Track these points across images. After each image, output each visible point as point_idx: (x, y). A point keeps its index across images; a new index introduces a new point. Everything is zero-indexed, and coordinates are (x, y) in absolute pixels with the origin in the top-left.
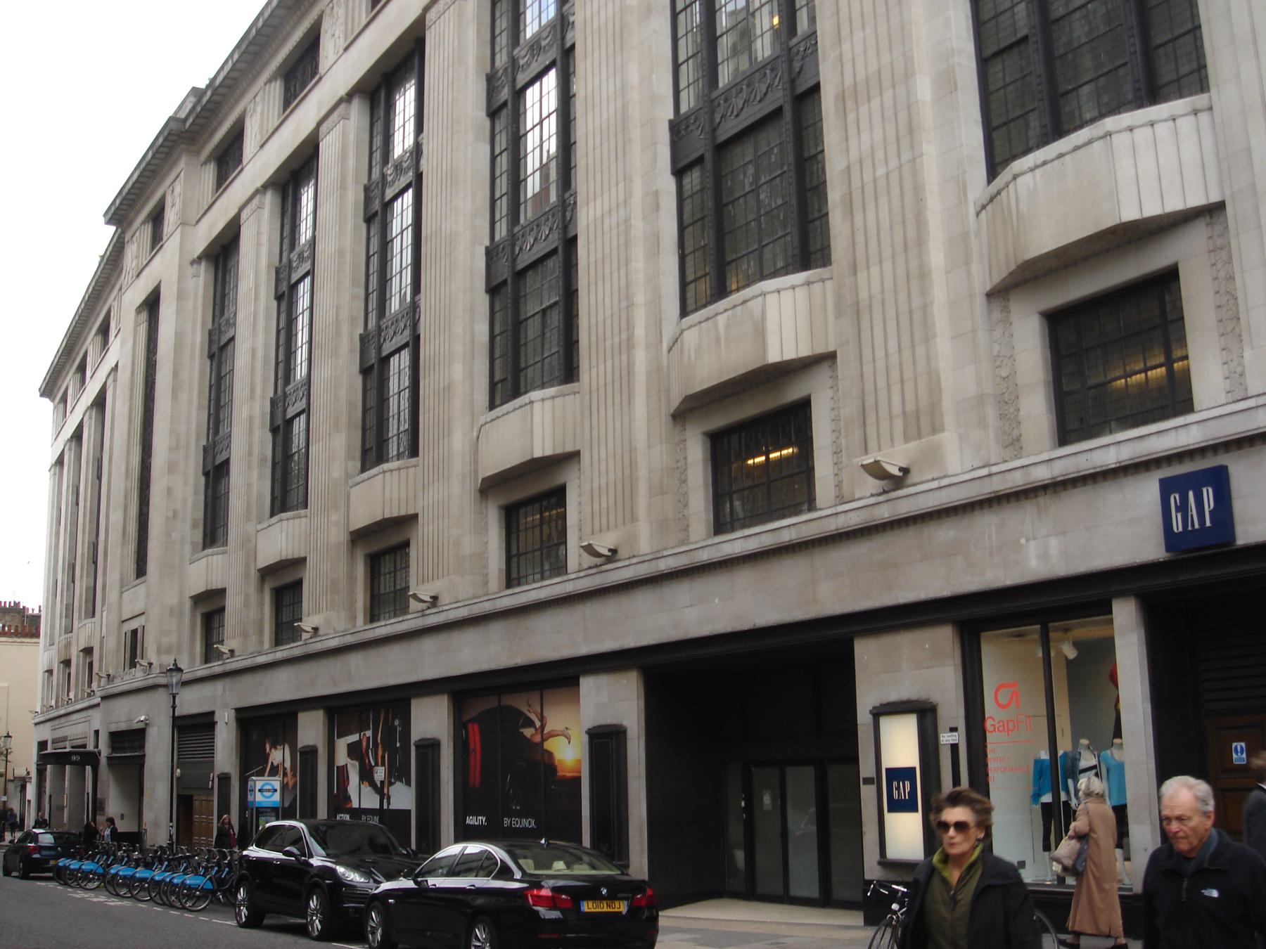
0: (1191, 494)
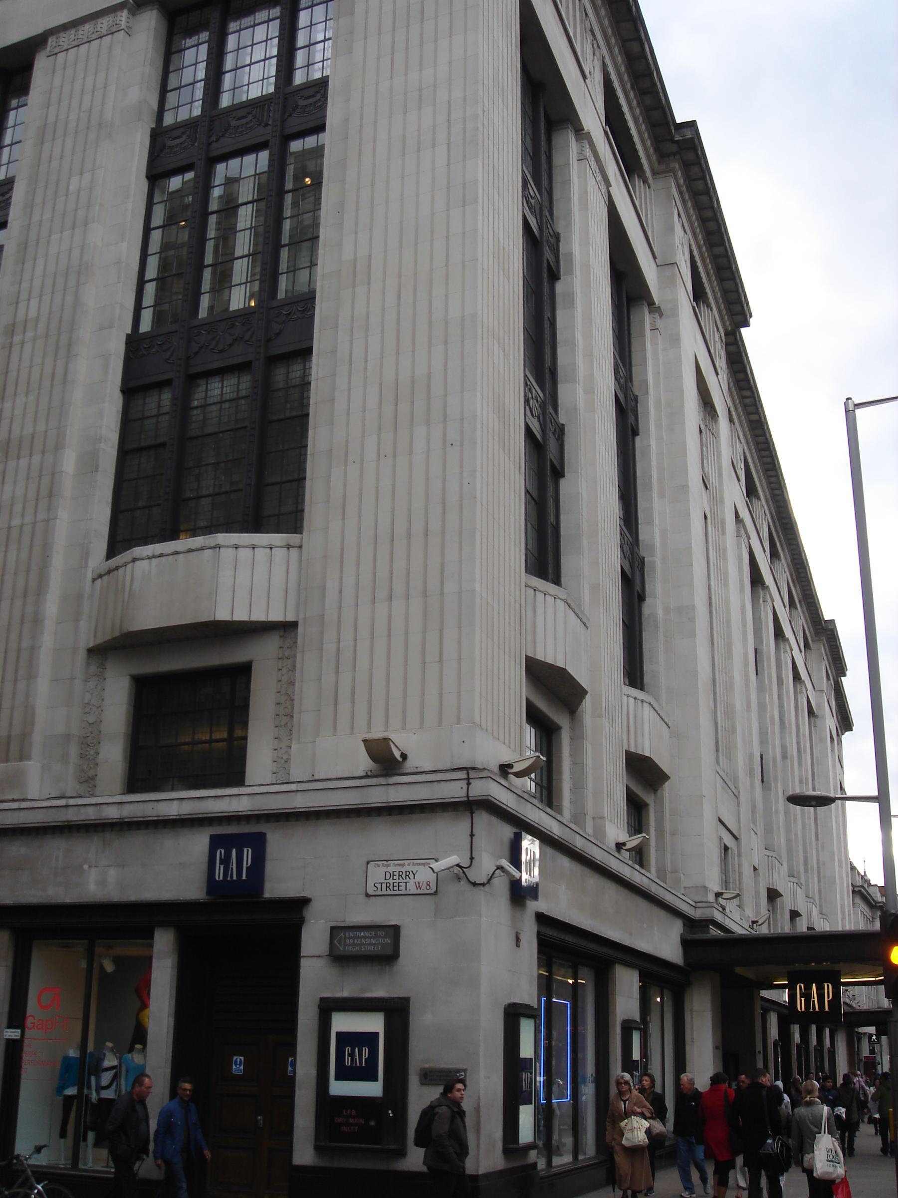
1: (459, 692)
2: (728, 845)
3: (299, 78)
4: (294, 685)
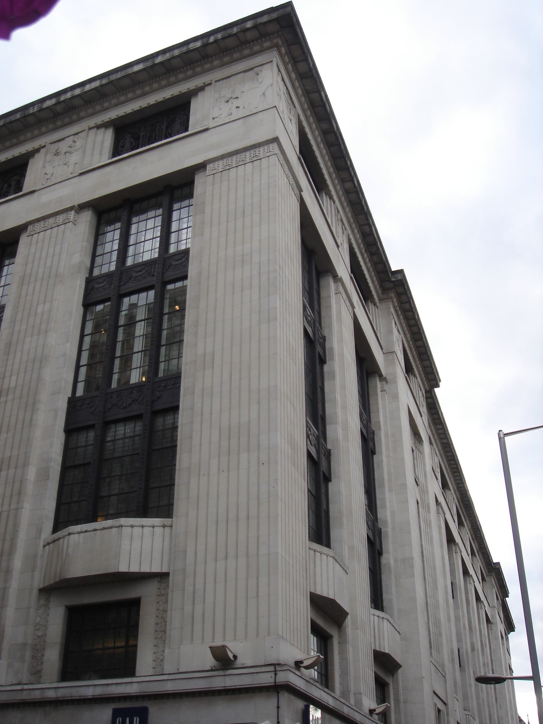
0: (128, 719)
1: (269, 616)
2: (440, 708)
3: (172, 249)
4: (167, 612)
